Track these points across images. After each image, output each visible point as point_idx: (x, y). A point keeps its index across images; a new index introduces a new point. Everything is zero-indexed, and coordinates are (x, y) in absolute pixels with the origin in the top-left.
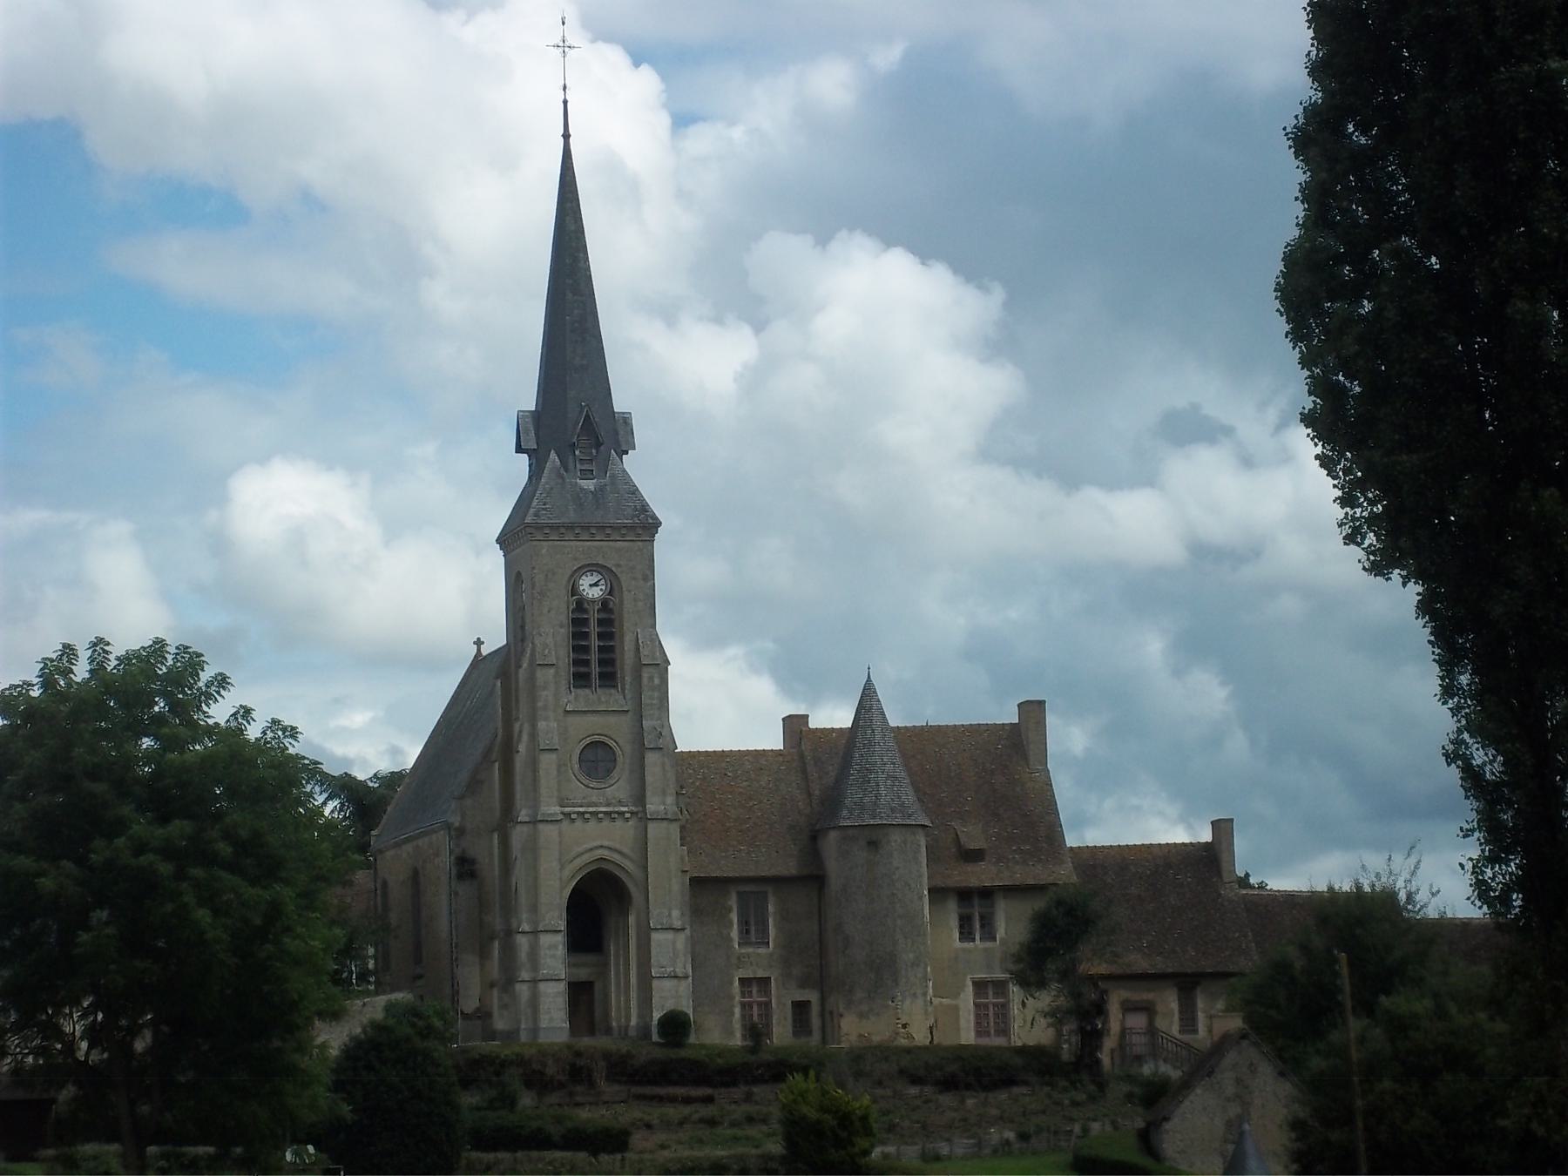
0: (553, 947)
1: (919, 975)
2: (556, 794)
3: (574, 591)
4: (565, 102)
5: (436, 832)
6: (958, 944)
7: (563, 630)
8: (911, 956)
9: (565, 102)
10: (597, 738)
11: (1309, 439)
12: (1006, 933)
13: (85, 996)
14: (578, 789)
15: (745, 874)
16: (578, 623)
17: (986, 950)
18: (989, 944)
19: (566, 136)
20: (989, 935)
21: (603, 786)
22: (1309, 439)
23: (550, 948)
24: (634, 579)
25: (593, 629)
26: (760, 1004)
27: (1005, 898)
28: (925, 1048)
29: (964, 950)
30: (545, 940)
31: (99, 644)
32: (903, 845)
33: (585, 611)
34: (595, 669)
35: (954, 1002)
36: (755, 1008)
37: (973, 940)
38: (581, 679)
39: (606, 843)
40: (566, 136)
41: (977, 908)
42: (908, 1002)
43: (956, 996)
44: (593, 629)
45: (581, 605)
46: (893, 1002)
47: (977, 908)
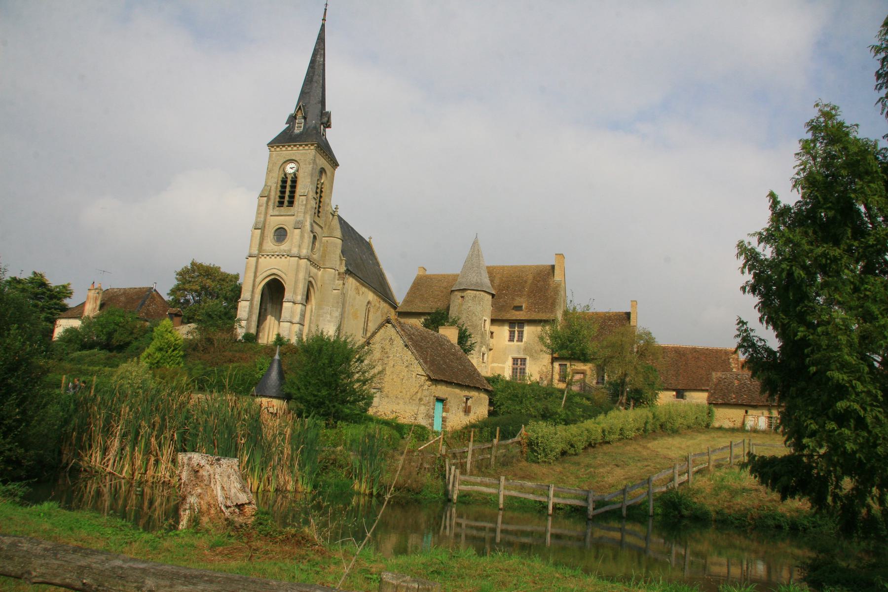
0: (245, 307)
4: (326, 9)
6: (507, 343)
9: (326, 9)
11: (818, 99)
15: (417, 311)
16: (284, 181)
17: (518, 345)
18: (519, 343)
19: (324, 20)
20: (520, 339)
22: (818, 99)
25: (289, 183)
29: (509, 345)
31: (785, 442)
35: (503, 365)
36: (519, 360)
40: (324, 20)
41: (516, 328)
43: (504, 362)
44: (289, 183)
47: (516, 328)
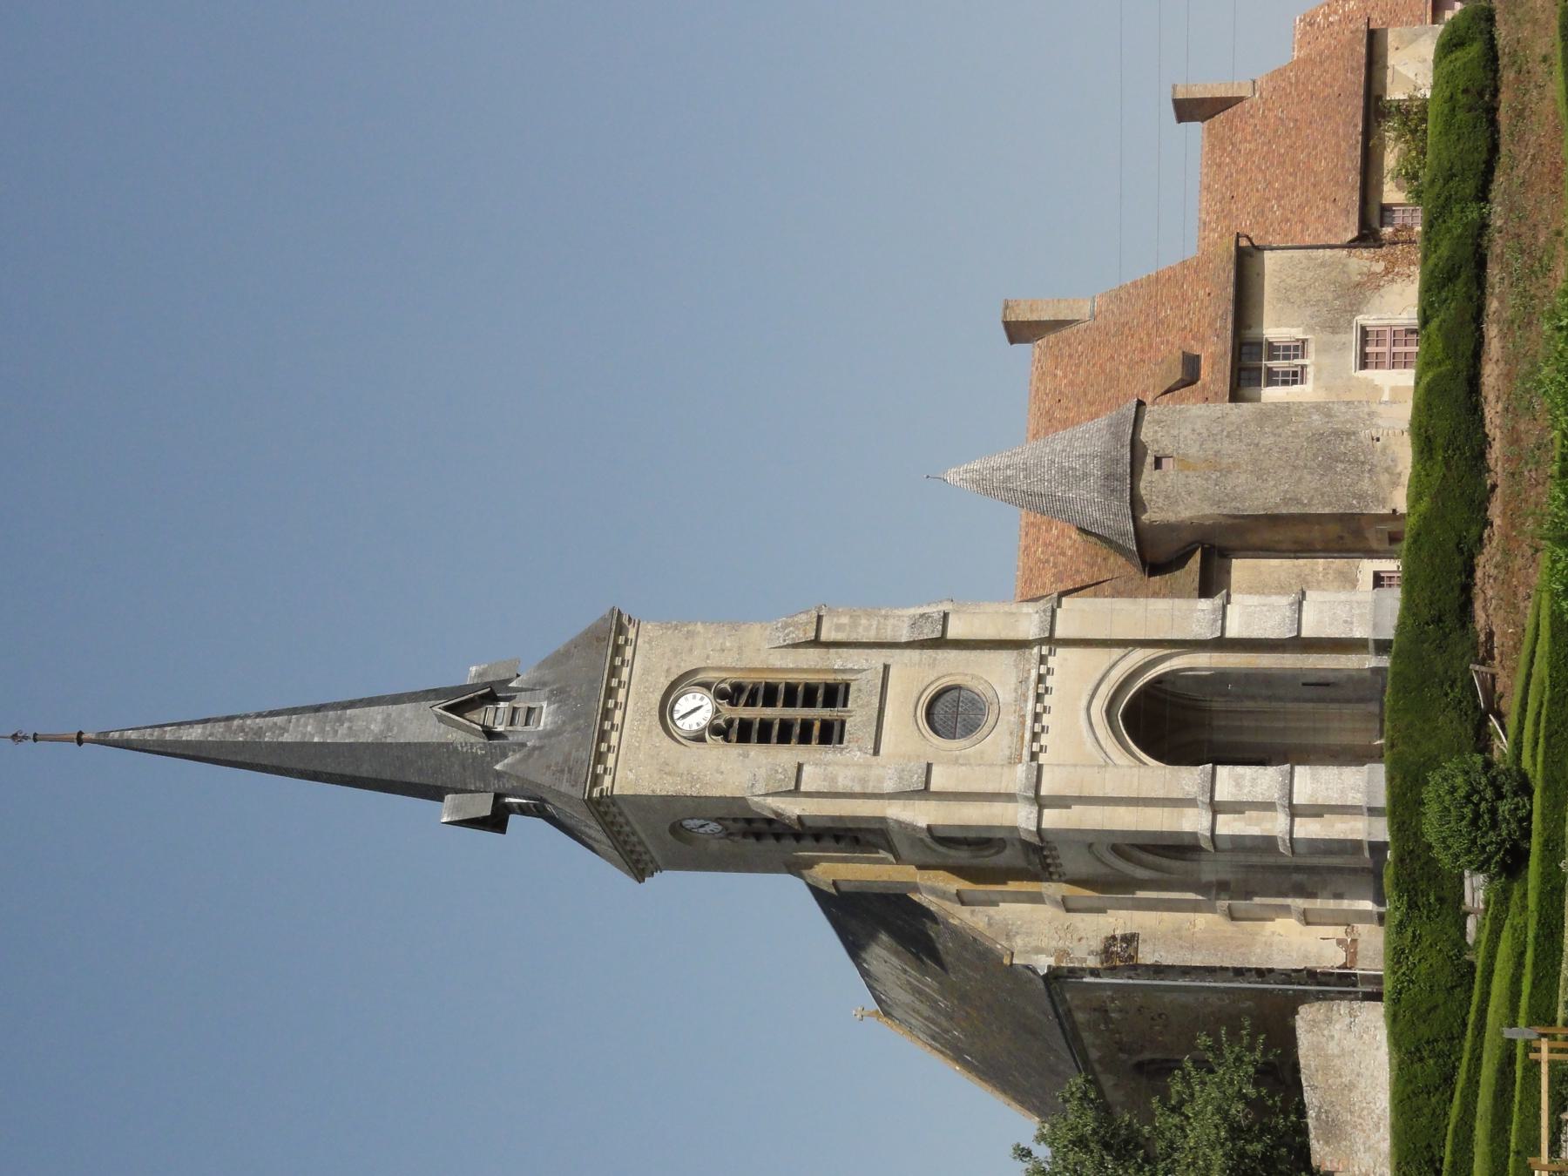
1: (1343, 409)
2: (998, 770)
3: (699, 738)
5: (1069, 1012)
7: (752, 754)
8: (1315, 417)
10: (921, 712)
12: (1299, 326)
13: (1511, 992)
14: (996, 740)
16: (745, 733)
21: (996, 707)
23: (1238, 785)
24: (691, 650)
25: (758, 713)
26: (1403, 213)
27: (1250, 327)
28: (1409, 607)
29: (1316, 379)
30: (1223, 793)
32: (1162, 425)
33: (730, 722)
34: (818, 713)
37: (1303, 367)
38: (830, 734)
39: (1084, 703)
42: (1380, 422)
44: (758, 713)
45: (720, 731)
46: (1378, 440)
